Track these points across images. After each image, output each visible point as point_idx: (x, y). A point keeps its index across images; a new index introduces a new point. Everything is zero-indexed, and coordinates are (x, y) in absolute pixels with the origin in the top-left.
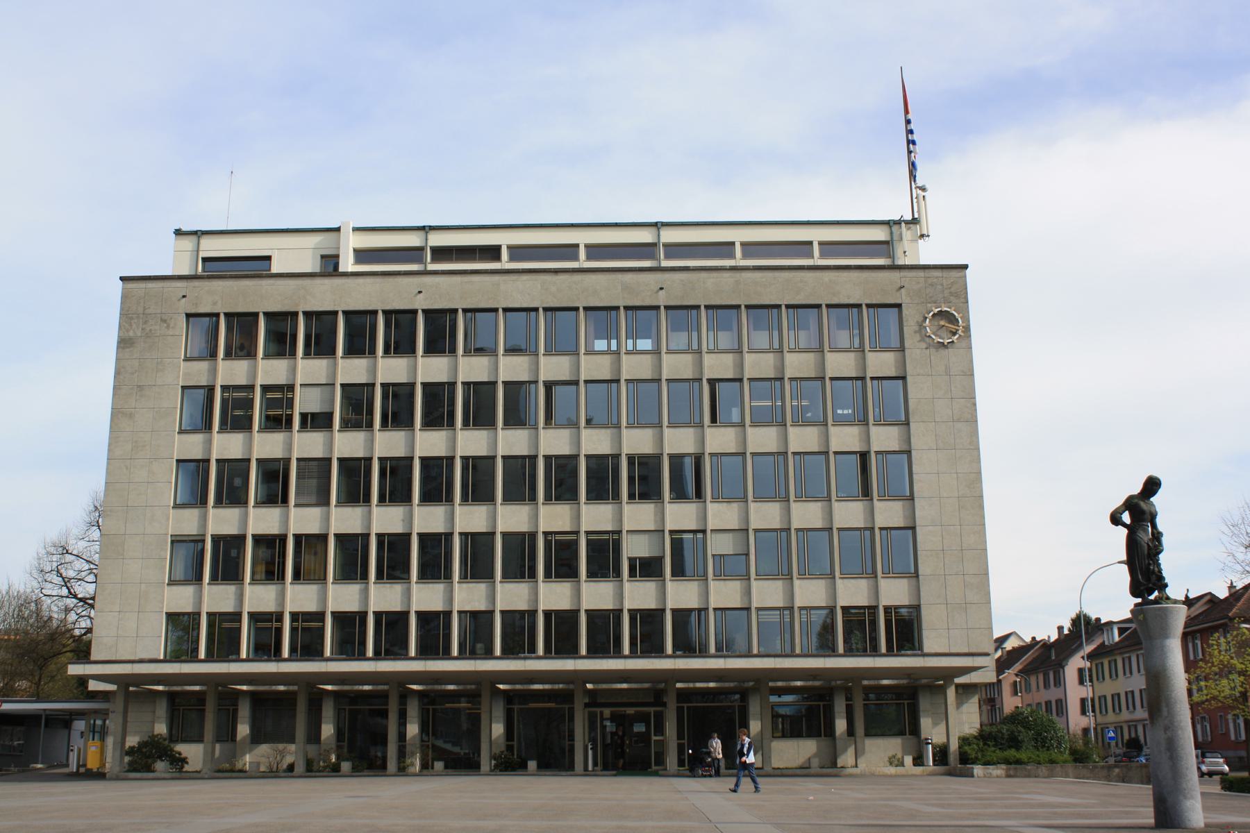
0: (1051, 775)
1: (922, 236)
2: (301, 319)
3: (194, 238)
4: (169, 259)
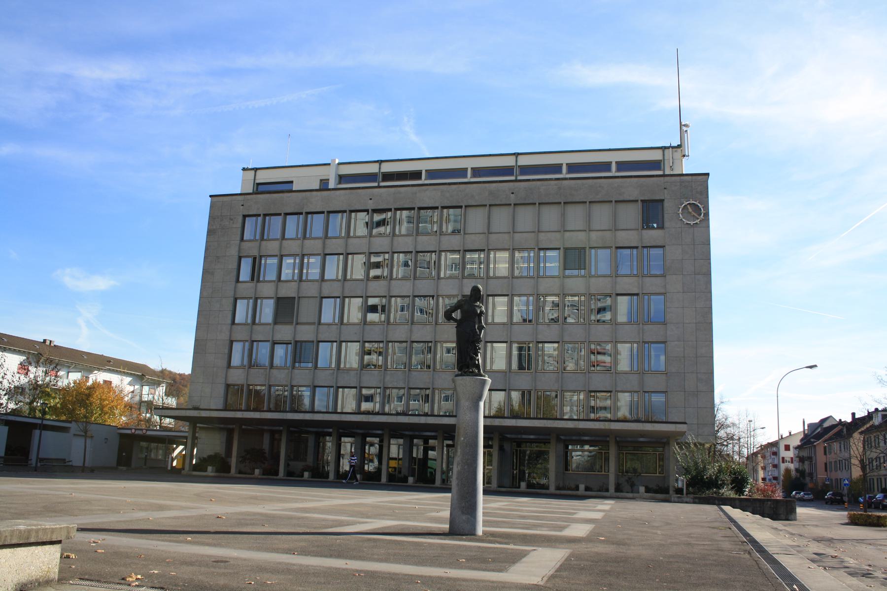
1: (684, 156)
3: (253, 172)
4: (235, 185)
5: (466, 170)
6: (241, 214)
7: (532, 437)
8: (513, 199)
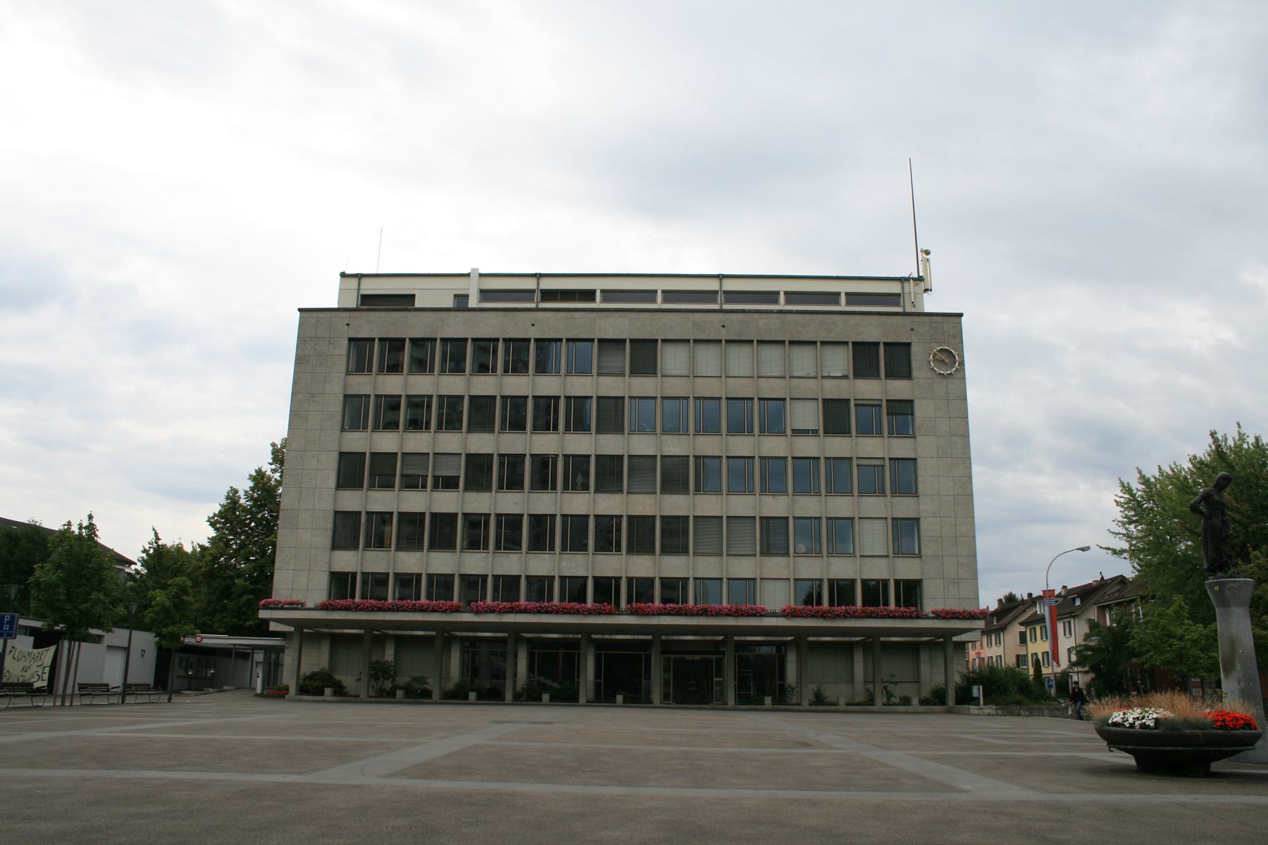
0: (1031, 715)
1: (926, 290)
2: (532, 346)
4: (329, 298)
5: (839, 294)
6: (346, 336)
7: (758, 638)
8: (723, 335)
